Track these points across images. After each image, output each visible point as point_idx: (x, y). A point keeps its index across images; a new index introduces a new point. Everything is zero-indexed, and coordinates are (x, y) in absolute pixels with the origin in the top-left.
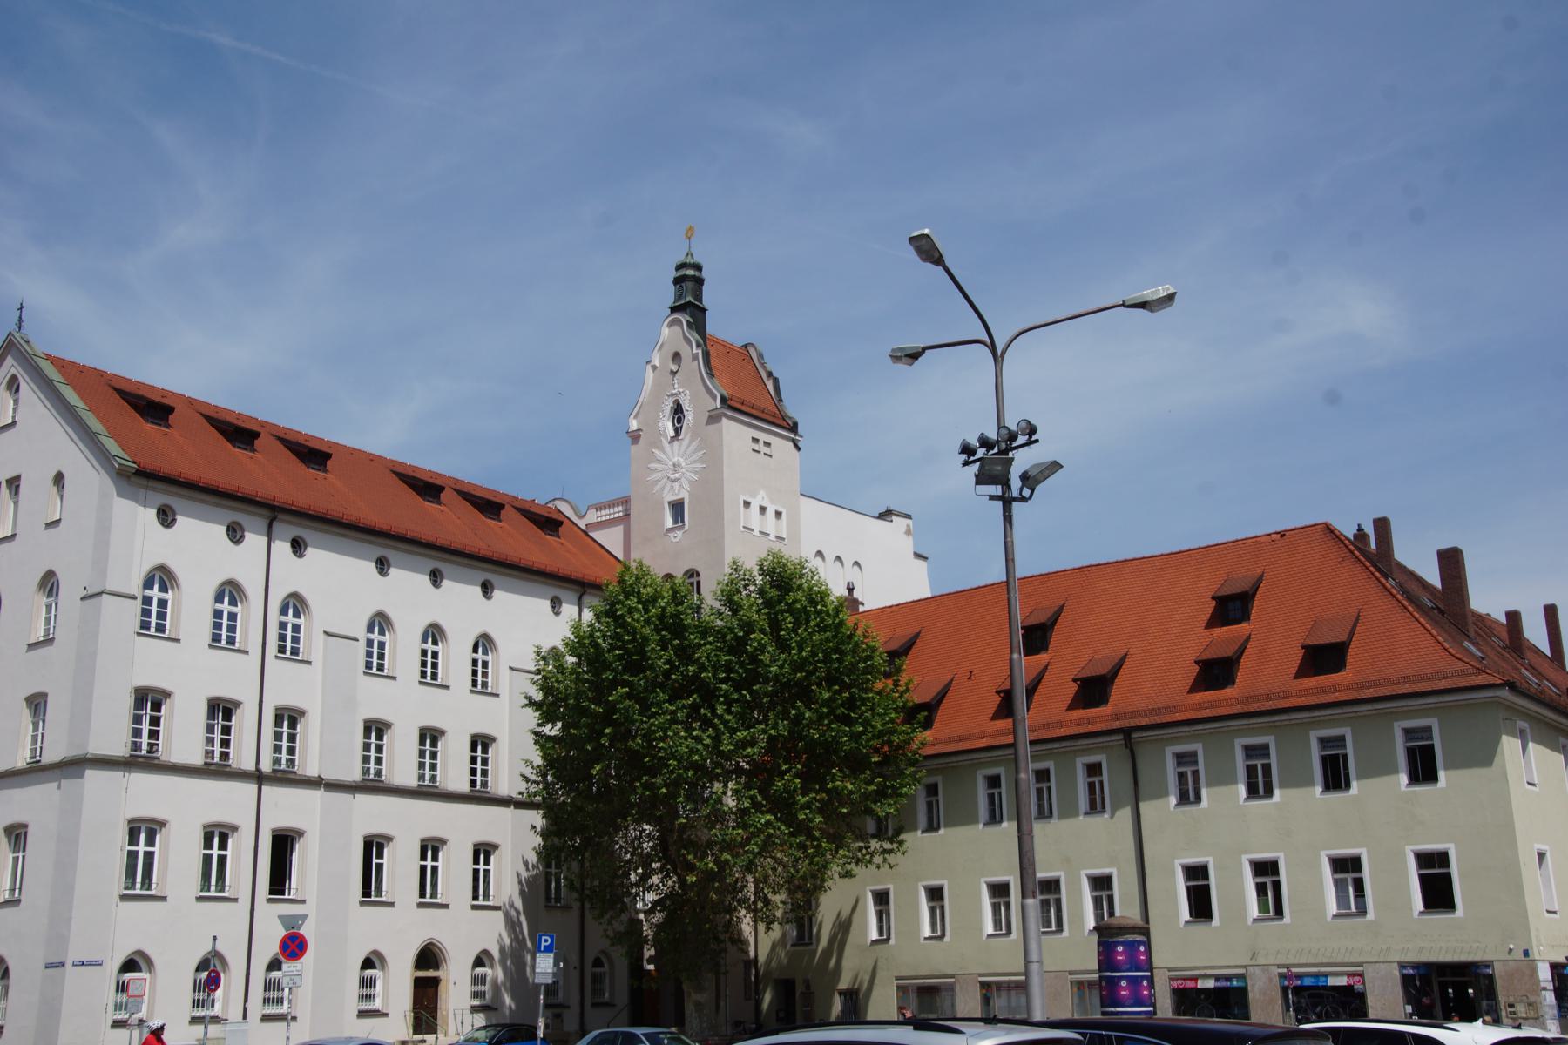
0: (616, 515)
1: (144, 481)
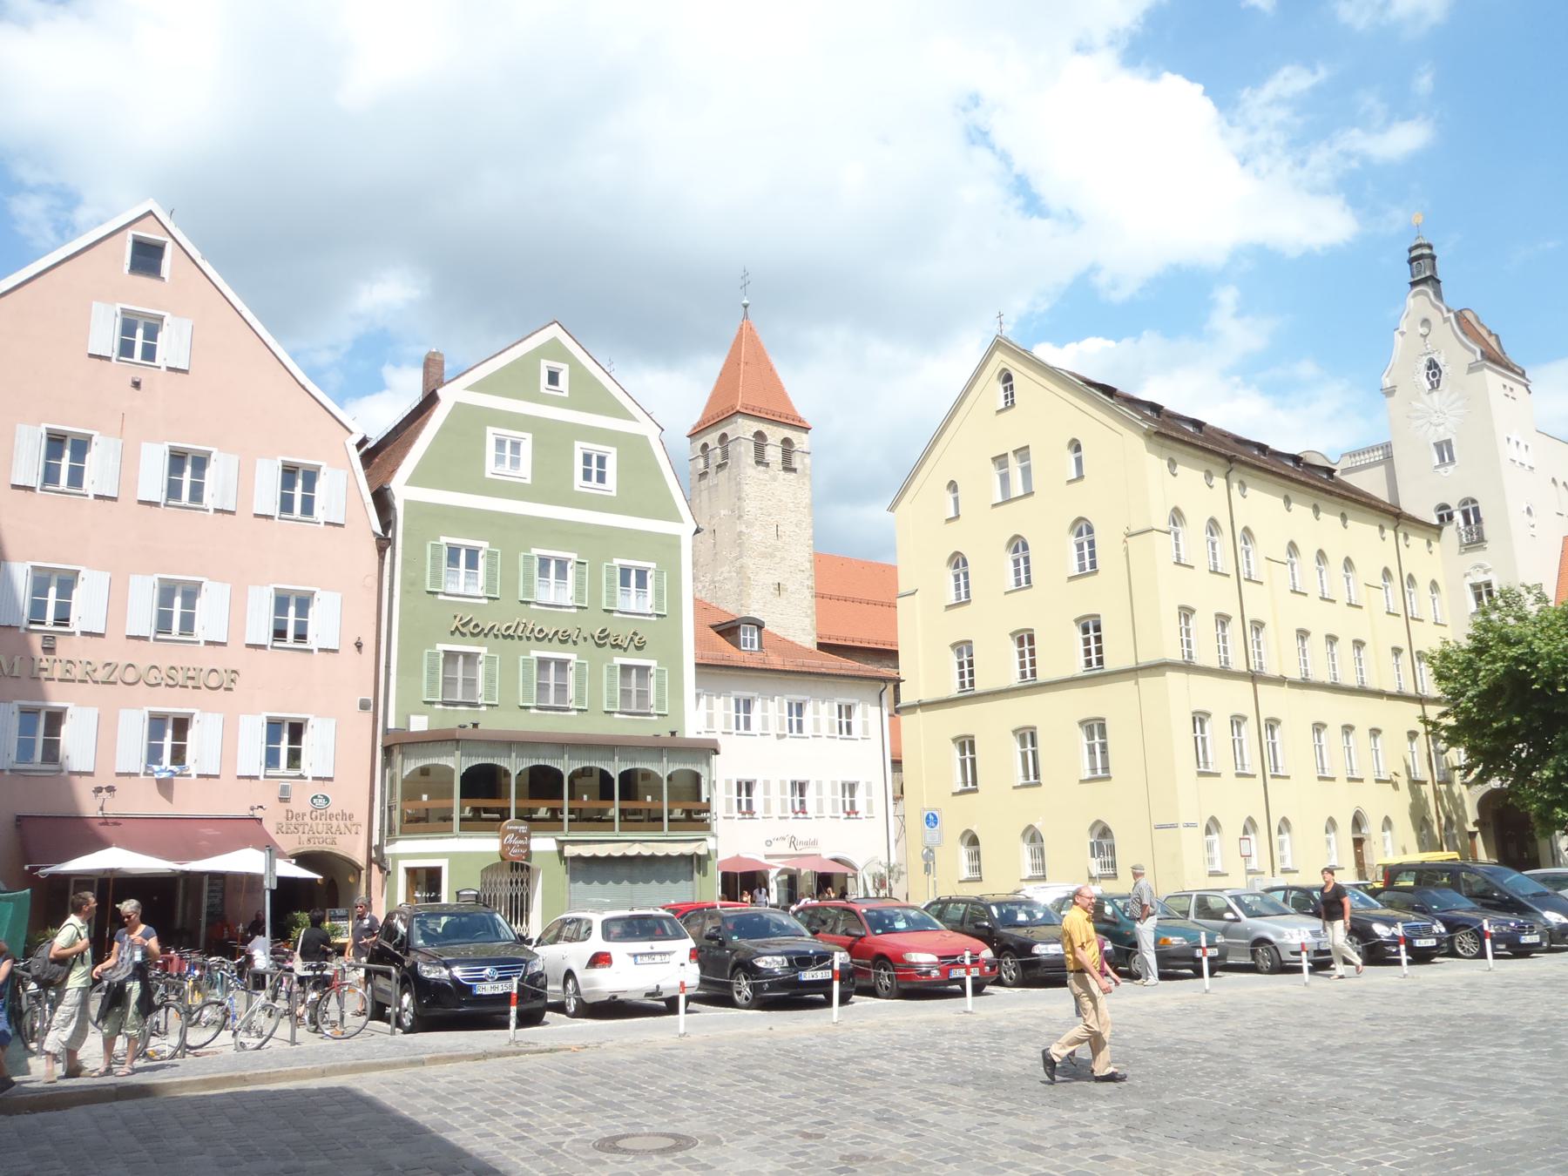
0: (1377, 459)
1: (1161, 440)
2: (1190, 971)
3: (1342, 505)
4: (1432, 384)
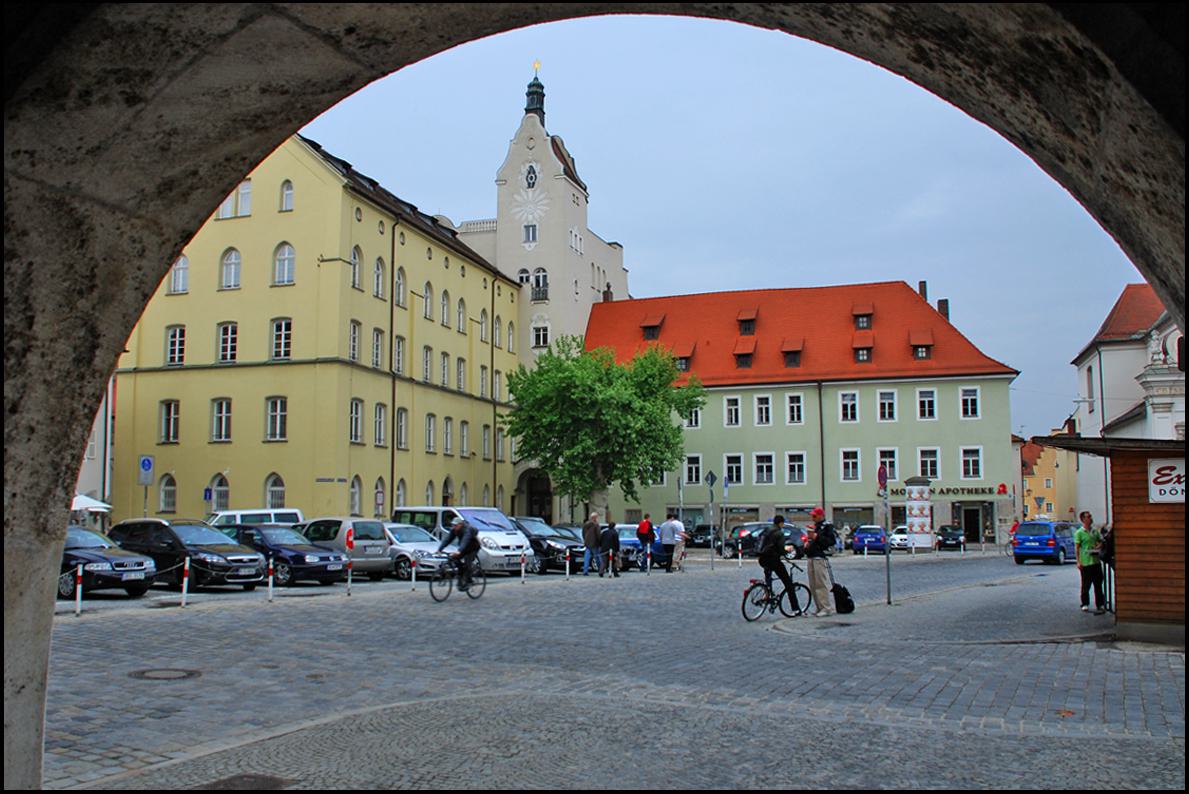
2: (317, 582)
3: (463, 260)
4: (529, 184)
